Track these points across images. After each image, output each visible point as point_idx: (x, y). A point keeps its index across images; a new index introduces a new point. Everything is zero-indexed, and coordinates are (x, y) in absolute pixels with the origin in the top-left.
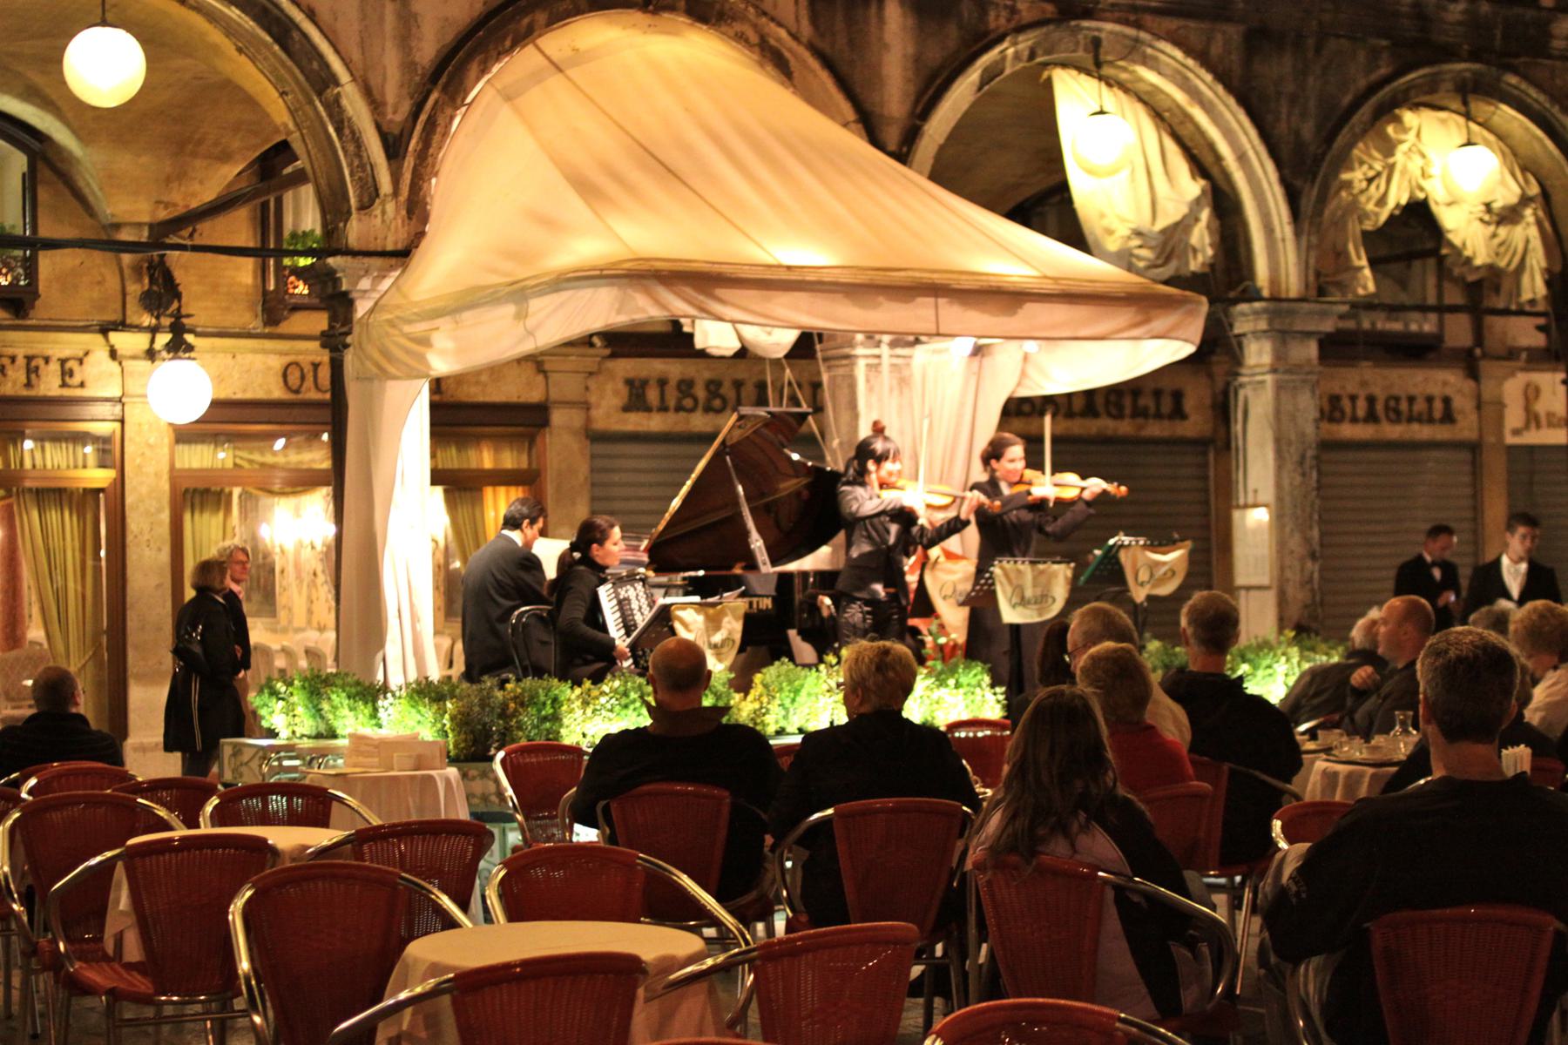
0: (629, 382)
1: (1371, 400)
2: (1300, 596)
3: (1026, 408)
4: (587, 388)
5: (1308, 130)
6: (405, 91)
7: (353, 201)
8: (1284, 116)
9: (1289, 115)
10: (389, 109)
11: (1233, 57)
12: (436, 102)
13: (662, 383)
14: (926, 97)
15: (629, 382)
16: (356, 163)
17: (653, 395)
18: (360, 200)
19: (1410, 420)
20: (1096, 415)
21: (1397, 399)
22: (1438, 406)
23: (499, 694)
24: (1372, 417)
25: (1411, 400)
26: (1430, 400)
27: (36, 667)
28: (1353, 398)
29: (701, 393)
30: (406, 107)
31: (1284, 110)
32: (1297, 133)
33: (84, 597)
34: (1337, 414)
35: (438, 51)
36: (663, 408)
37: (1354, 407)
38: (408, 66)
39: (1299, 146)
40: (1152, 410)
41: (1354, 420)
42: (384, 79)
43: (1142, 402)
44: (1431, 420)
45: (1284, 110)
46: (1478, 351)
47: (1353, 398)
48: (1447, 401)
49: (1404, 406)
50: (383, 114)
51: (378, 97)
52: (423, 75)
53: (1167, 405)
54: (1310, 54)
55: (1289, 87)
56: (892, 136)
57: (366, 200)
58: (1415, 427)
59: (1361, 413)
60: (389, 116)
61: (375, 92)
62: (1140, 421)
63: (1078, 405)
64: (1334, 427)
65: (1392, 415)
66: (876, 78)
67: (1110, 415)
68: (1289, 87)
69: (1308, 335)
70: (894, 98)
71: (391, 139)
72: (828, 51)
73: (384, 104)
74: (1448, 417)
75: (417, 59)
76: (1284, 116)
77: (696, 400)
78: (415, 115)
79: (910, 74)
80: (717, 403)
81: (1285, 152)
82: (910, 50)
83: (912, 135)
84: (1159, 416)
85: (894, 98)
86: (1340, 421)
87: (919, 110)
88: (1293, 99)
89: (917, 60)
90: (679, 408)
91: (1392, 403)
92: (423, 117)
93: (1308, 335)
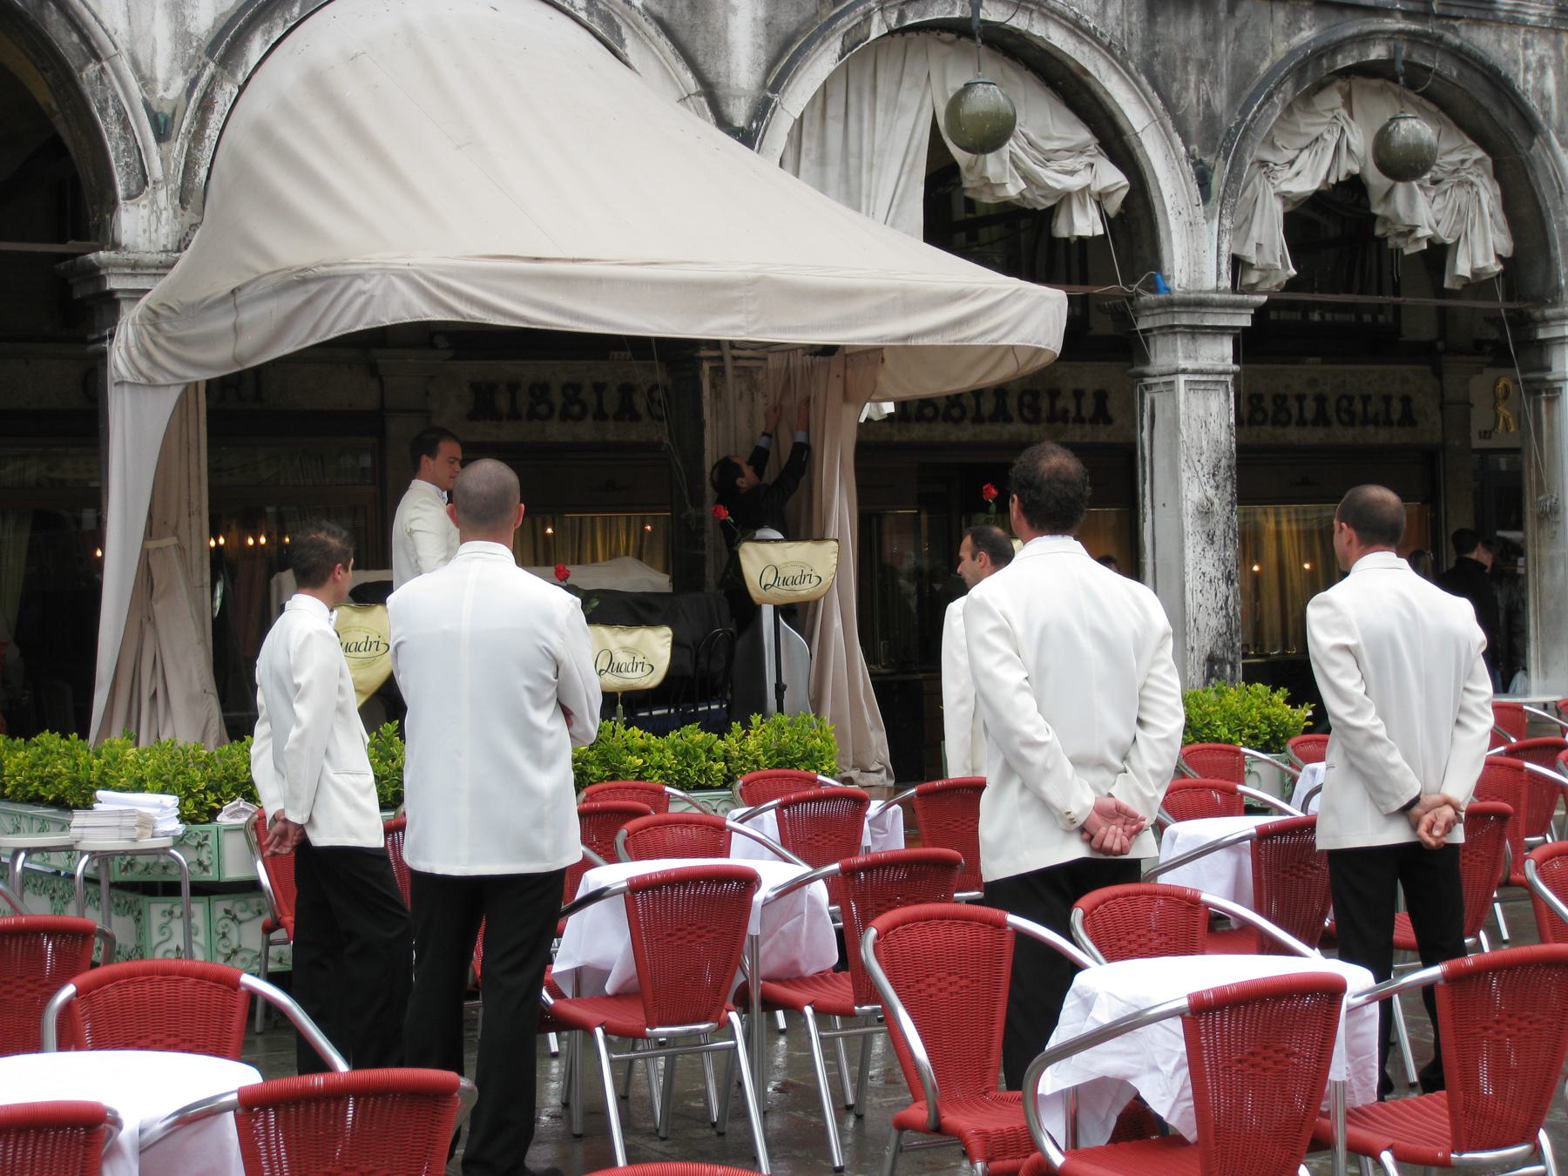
0: (475, 387)
1: (1321, 400)
2: (1213, 622)
3: (929, 412)
4: (427, 394)
5: (1220, 101)
6: (177, 66)
7: (120, 191)
8: (1192, 85)
9: (1199, 82)
10: (160, 87)
11: (1134, 19)
12: (213, 77)
13: (513, 387)
14: (778, 69)
15: (475, 387)
16: (122, 147)
17: (502, 402)
18: (127, 189)
19: (1365, 422)
20: (1009, 420)
21: (1350, 399)
22: (1396, 405)
23: (721, 743)
24: (1321, 419)
25: (1366, 399)
26: (1387, 399)
27: (340, 710)
28: (1301, 398)
29: (558, 399)
30: (180, 83)
31: (1193, 78)
32: (1208, 104)
33: (1153, 507)
34: (1283, 417)
35: (216, 20)
36: (514, 415)
37: (1301, 409)
38: (182, 37)
39: (1210, 119)
40: (1072, 414)
41: (1302, 422)
42: (154, 51)
43: (1060, 404)
44: (1389, 423)
45: (1193, 78)
46: (1440, 345)
47: (1301, 398)
48: (1406, 400)
49: (1358, 406)
50: (153, 92)
51: (147, 73)
52: (198, 48)
53: (1088, 407)
54: (1222, 15)
55: (1199, 52)
56: (740, 114)
57: (133, 187)
58: (1371, 429)
59: (1309, 414)
60: (160, 93)
61: (143, 67)
62: (1059, 424)
63: (988, 406)
64: (1279, 431)
65: (1344, 417)
66: (720, 45)
67: (1025, 420)
68: (1199, 52)
69: (1219, 331)
70: (742, 67)
71: (162, 120)
72: (666, 16)
73: (154, 80)
74: (1408, 419)
75: (191, 30)
76: (1192, 85)
77: (1266, 415)
78: (189, 92)
79: (761, 40)
80: (576, 409)
81: (1194, 125)
82: (761, 13)
83: (763, 109)
84: (1079, 420)
85: (742, 67)
86: (1286, 424)
87: (770, 82)
88: (1203, 67)
89: (769, 23)
90: (532, 415)
91: (1345, 403)
92: (197, 94)
93: (1219, 331)
